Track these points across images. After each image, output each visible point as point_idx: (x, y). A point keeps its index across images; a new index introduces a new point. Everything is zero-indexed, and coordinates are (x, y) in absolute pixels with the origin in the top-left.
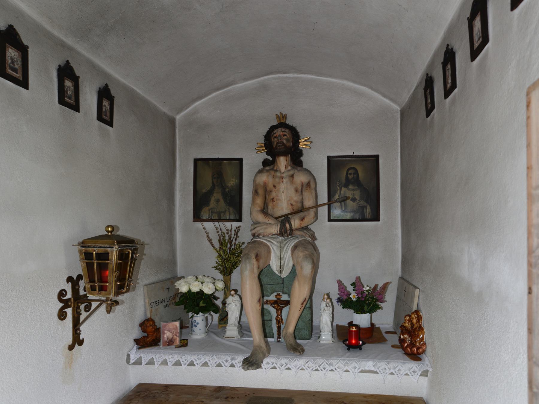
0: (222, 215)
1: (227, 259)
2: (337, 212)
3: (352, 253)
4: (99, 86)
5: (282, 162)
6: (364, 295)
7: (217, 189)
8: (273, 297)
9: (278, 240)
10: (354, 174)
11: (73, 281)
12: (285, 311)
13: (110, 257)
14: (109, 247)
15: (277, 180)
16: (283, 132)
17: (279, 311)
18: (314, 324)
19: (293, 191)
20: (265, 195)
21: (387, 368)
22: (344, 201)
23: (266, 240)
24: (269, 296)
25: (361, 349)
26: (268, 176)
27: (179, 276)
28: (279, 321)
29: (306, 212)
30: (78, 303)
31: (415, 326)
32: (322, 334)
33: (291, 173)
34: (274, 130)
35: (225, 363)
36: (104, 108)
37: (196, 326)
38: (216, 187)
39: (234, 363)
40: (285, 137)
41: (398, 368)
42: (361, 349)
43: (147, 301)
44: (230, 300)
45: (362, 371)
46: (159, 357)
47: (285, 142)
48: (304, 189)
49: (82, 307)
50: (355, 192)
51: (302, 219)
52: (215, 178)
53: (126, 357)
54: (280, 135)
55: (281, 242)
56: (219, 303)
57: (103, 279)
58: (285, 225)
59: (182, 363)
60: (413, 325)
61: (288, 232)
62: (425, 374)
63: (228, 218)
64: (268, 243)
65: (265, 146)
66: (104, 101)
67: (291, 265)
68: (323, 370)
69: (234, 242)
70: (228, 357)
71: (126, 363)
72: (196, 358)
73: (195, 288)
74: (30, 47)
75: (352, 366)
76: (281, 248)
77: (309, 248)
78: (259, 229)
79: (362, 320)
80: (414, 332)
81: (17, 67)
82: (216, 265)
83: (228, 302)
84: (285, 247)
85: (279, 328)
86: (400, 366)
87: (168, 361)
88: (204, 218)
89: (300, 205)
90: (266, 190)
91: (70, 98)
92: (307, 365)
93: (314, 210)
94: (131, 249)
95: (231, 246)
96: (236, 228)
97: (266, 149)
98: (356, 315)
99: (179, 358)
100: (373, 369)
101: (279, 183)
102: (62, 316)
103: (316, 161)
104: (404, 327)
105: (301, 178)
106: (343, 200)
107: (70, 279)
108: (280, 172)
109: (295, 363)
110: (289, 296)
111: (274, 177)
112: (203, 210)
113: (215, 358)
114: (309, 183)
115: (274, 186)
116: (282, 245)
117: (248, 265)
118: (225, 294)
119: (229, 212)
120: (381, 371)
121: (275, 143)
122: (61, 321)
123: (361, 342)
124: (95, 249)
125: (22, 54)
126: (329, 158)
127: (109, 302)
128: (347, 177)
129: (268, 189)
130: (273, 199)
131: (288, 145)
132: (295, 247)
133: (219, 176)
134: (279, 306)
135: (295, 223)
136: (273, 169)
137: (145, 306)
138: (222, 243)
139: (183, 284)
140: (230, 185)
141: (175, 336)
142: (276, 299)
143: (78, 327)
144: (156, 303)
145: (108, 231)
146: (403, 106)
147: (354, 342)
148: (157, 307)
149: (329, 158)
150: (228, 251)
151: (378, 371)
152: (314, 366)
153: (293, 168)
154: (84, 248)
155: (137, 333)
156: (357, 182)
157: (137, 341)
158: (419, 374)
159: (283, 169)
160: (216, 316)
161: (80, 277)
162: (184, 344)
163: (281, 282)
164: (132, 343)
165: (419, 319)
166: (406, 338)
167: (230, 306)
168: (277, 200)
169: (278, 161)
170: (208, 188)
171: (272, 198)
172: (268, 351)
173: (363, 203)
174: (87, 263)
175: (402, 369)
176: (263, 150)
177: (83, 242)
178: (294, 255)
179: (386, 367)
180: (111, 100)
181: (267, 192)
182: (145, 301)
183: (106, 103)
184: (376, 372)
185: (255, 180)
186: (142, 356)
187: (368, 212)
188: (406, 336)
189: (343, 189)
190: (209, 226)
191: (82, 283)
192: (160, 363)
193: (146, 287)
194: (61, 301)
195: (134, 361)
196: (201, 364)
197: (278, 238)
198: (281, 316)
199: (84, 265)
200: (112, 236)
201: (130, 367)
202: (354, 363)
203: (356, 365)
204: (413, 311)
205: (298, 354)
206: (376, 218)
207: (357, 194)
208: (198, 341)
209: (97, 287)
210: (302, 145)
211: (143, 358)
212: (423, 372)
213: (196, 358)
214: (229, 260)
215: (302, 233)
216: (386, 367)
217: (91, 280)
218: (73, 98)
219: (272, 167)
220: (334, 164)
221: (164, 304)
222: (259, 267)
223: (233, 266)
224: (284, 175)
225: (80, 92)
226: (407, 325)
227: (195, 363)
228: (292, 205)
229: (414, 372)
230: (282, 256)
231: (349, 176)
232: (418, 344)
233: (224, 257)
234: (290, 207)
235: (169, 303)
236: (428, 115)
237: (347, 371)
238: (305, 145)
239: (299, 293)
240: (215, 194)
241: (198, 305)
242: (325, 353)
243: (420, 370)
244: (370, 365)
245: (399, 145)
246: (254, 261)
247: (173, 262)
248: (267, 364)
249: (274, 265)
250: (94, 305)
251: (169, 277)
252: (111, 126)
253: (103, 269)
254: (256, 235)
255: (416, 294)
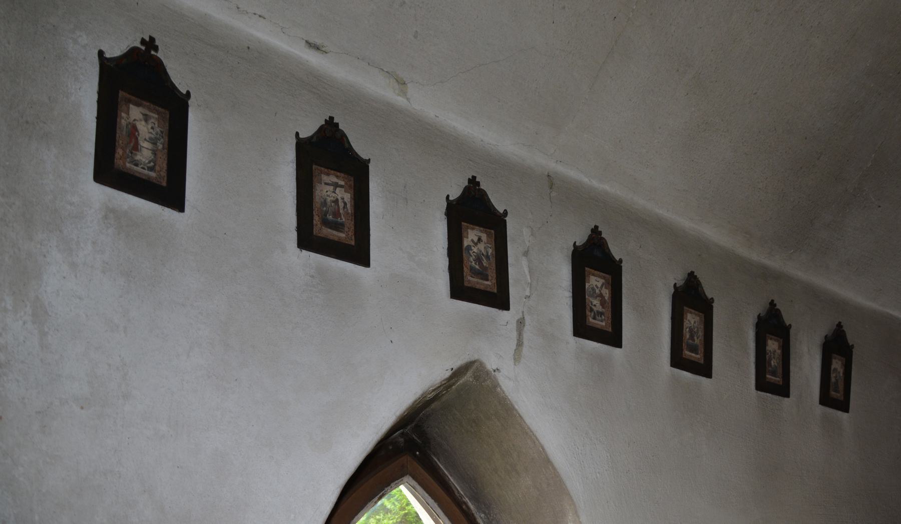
4: (824, 334)
36: (833, 375)
66: (834, 361)
74: (715, 301)
81: (697, 341)
91: (774, 373)
125: (705, 317)
225: (792, 356)
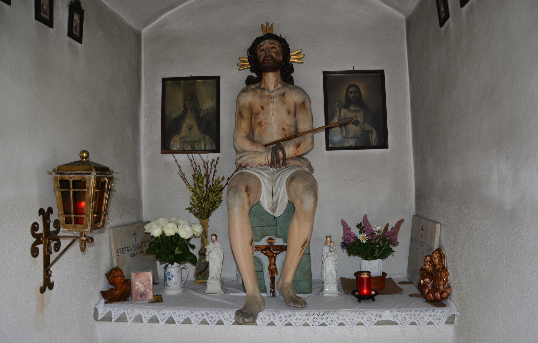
0: (196, 144)
1: (204, 198)
2: (337, 136)
3: (358, 187)
5: (271, 79)
6: (375, 236)
7: (190, 113)
8: (264, 242)
9: (268, 171)
10: (355, 92)
11: (45, 214)
12: (280, 258)
13: (87, 185)
14: (87, 174)
15: (266, 100)
16: (271, 44)
17: (272, 257)
18: (313, 278)
19: (285, 112)
20: (250, 118)
21: (407, 317)
22: (345, 125)
23: (255, 171)
24: (259, 241)
25: (373, 300)
26: (254, 96)
27: (144, 221)
28: (273, 271)
29: (301, 137)
30: (49, 239)
31: (438, 267)
32: (325, 285)
33: (282, 91)
34: (260, 43)
35: (211, 319)
36: (74, 23)
37: (170, 279)
38: (189, 111)
39: (223, 319)
40: (274, 50)
41: (420, 316)
42: (373, 300)
43: (113, 247)
44: (210, 247)
45: (379, 323)
46: (132, 311)
47: (274, 55)
48: (297, 111)
49: (52, 245)
50: (357, 114)
51: (298, 146)
52: (187, 100)
53: (93, 311)
54: (267, 48)
55: (272, 174)
56: (195, 252)
57: (78, 211)
58: (277, 153)
59: (159, 319)
60: (434, 266)
61: (281, 161)
62: (450, 321)
63: (203, 149)
64: (257, 175)
65: (249, 61)
66: (75, 15)
67: (286, 200)
68: (331, 323)
69: (211, 176)
70: (214, 312)
71: (93, 319)
72: (176, 314)
73: (170, 232)
75: (366, 317)
76: (273, 182)
77: (305, 178)
78: (246, 159)
79: (374, 267)
80: (436, 274)
82: (190, 206)
83: (208, 250)
84: (278, 180)
85: (273, 279)
86: (422, 314)
87: (143, 316)
88: (175, 149)
89: (293, 129)
90: (252, 113)
91: (45, 13)
92: (312, 318)
93: (311, 134)
94: (106, 177)
95: (208, 182)
96: (213, 161)
97: (250, 64)
98: (364, 261)
99: (156, 313)
100: (391, 319)
101: (268, 104)
102: (34, 252)
103: (309, 78)
104: (425, 270)
105: (293, 98)
106: (343, 125)
107: (41, 212)
108: (269, 90)
109: (296, 317)
110: (285, 240)
111: (261, 96)
112: (173, 140)
113: (199, 313)
114: (303, 104)
115: (262, 107)
116: (274, 178)
117: (237, 199)
118: (202, 241)
119: (205, 140)
120: (401, 321)
121: (262, 57)
122: (33, 258)
123: (373, 293)
124: (72, 176)
126: (325, 74)
127: (84, 238)
128: (347, 96)
129: (254, 111)
130: (260, 123)
131: (277, 59)
132: (292, 178)
133: (192, 98)
134: (272, 252)
135: (290, 150)
136: (259, 87)
137: (111, 253)
138: (197, 177)
139: (155, 226)
140: (205, 109)
141: (148, 290)
142: (268, 244)
143: (48, 268)
144: (123, 250)
145: (82, 157)
146: (409, 14)
147: (365, 292)
148: (123, 256)
149: (325, 74)
150: (205, 189)
151: (397, 321)
152: (320, 320)
153: (284, 86)
154: (59, 176)
155: (103, 285)
156: (359, 102)
157: (104, 294)
158: (445, 321)
159: (271, 87)
160: (190, 269)
161: (50, 210)
162: (158, 299)
163: (273, 223)
164: (98, 296)
165: (442, 257)
166: (428, 283)
167: (211, 255)
168: (265, 123)
169: (265, 77)
170: (179, 112)
171: (259, 121)
172: (262, 305)
173: (367, 127)
174: (62, 192)
175: (425, 317)
176: (247, 65)
177: (59, 168)
178: (291, 188)
179: (406, 316)
180: (81, 13)
181: (253, 114)
182: (111, 248)
183: (76, 17)
184: (395, 323)
185: (237, 101)
186: (112, 310)
187: (374, 137)
188: (427, 280)
189: (343, 111)
190: (182, 158)
191: (53, 218)
192: (133, 319)
193: (111, 229)
194: (34, 235)
195: (102, 317)
196: (183, 320)
197: (268, 169)
198: (275, 265)
199: (59, 194)
200: (84, 163)
201: (97, 324)
202: (368, 314)
203: (371, 316)
204: (435, 250)
205: (300, 306)
206: (383, 144)
207: (360, 116)
208: (174, 296)
209: (73, 219)
210: (293, 59)
211: (113, 313)
212: (449, 318)
213: (176, 314)
214: (206, 201)
215: (298, 163)
216: (406, 316)
217: (66, 211)
218: (48, 13)
219: (258, 85)
220: (331, 80)
221: (132, 252)
222: (249, 203)
223: (212, 207)
224: (274, 94)
226: (427, 267)
227: (175, 319)
228: (283, 129)
229: (439, 319)
230: (274, 191)
231: (349, 94)
232: (441, 288)
233: (201, 195)
234: (281, 132)
235: (136, 252)
236: (442, 23)
237: (360, 324)
238: (296, 59)
239: (298, 233)
240: (187, 120)
241: (173, 252)
242: (332, 305)
243: (445, 316)
244: (387, 315)
245: (407, 58)
246: (244, 195)
247: (137, 204)
248: (263, 319)
249: (266, 202)
250: (64, 243)
251: (135, 221)
252: (80, 41)
253: (78, 198)
254: (243, 165)
255: (437, 230)
